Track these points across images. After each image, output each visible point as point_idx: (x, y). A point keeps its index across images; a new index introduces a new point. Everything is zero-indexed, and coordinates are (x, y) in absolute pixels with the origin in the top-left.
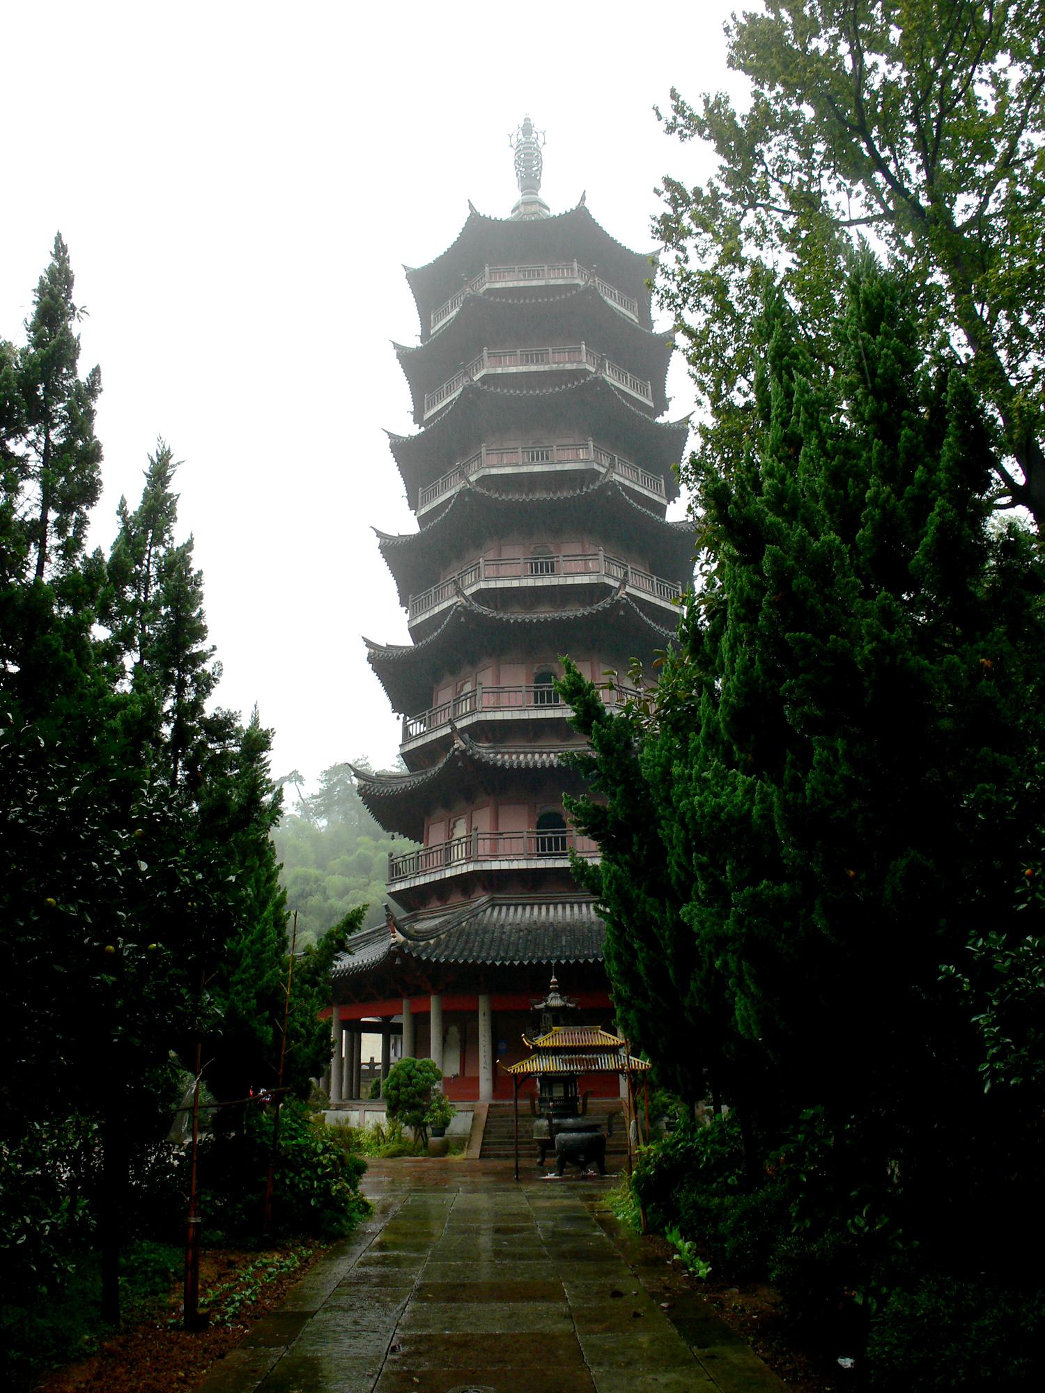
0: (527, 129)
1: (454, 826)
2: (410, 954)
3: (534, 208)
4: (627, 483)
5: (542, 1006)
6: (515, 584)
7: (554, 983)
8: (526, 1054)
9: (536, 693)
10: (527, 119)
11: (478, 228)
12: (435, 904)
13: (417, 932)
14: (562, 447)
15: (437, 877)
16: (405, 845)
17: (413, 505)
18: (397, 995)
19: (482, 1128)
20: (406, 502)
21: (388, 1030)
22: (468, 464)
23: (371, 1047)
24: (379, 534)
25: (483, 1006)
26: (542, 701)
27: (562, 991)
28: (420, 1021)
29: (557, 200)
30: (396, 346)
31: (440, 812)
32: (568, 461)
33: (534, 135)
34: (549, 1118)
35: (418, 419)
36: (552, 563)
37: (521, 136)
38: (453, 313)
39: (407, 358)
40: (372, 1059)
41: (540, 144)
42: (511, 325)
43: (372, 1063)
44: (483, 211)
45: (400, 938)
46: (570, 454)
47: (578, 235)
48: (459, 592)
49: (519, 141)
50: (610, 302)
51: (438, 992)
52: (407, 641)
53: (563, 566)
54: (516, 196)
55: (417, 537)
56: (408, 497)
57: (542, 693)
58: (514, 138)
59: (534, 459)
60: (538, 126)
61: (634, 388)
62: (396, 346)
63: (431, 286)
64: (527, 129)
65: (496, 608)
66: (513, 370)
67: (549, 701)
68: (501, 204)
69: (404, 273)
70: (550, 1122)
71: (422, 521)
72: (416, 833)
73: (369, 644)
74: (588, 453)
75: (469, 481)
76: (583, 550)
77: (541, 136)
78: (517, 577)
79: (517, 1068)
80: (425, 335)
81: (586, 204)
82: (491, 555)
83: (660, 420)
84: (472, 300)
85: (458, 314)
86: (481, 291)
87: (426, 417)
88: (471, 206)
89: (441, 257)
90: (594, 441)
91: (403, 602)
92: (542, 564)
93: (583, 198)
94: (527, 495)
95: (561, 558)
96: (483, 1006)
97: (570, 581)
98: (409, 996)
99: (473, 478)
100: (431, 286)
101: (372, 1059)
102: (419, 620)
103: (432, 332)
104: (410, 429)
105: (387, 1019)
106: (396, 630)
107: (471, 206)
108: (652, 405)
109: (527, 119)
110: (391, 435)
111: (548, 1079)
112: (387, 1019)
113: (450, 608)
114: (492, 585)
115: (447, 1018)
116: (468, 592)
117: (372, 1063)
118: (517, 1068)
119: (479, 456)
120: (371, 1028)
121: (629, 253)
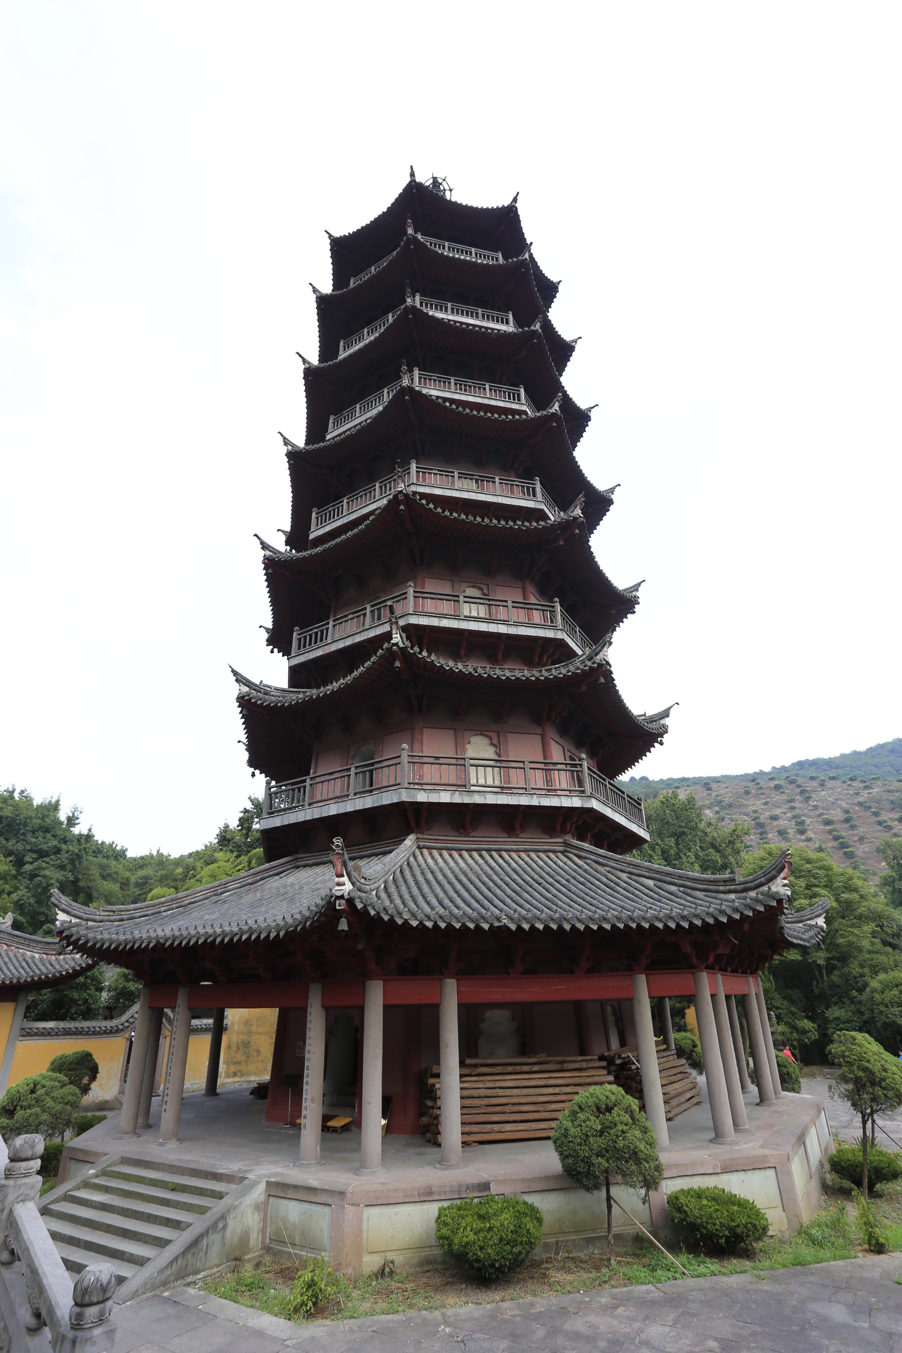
44: (337, 234)
69: (285, 450)
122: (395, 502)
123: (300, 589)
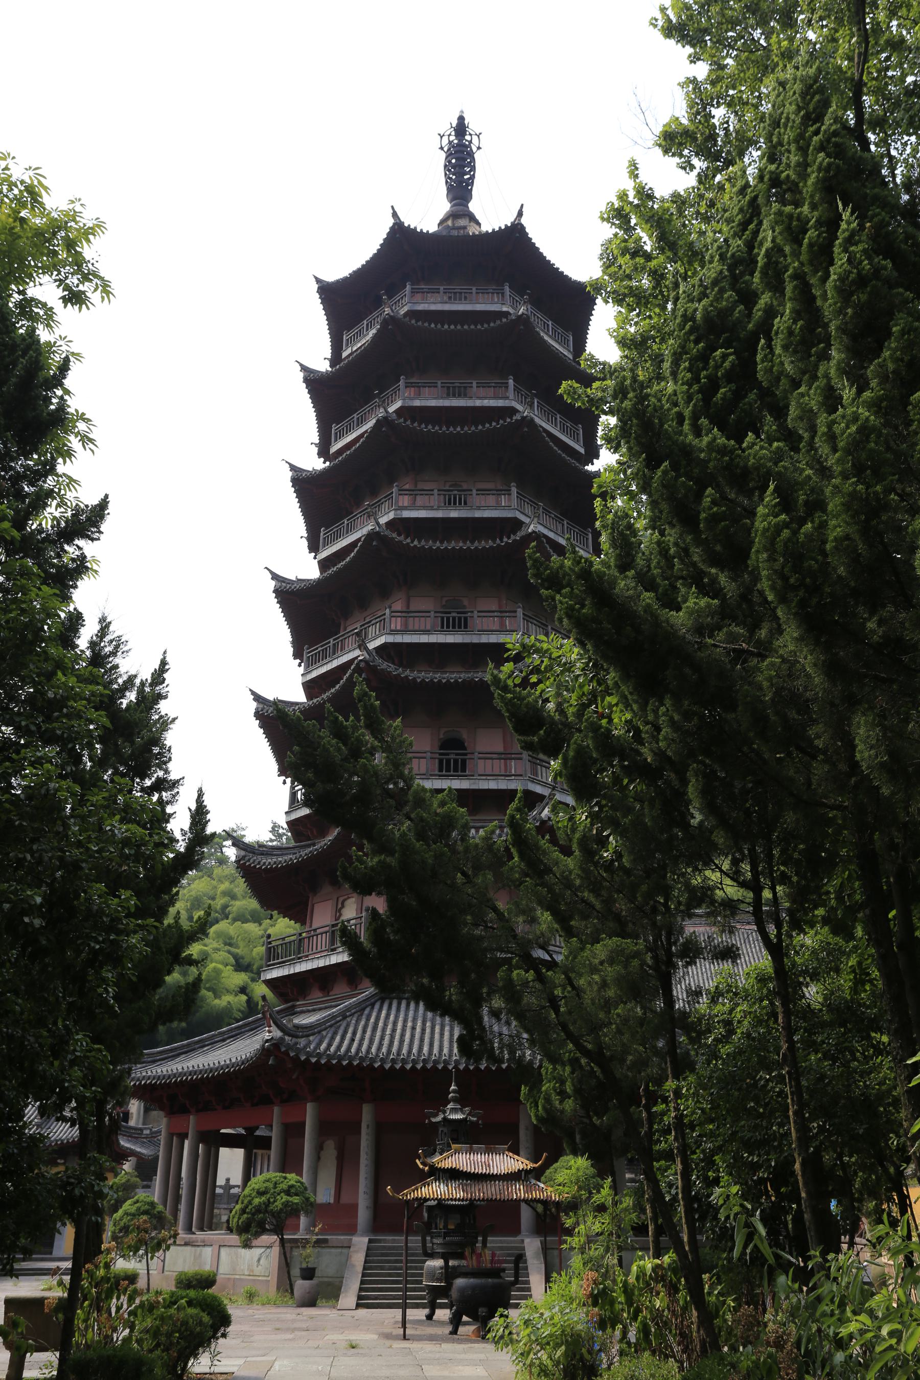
0: (461, 128)
1: (343, 906)
2: (286, 1053)
3: (462, 222)
4: (551, 535)
5: (440, 1118)
6: (424, 639)
7: (454, 1091)
8: (422, 1177)
9: (441, 762)
10: (461, 119)
11: (401, 237)
12: (316, 995)
13: (297, 1027)
14: (483, 492)
15: (321, 963)
16: (283, 927)
17: (314, 547)
18: (266, 1101)
19: (360, 1269)
20: (316, 450)
21: (252, 1145)
22: (378, 505)
23: (231, 1163)
24: (293, 468)
25: (367, 1114)
26: (448, 770)
27: (463, 1101)
28: (293, 1131)
29: (490, 213)
30: (304, 368)
31: (327, 889)
32: (488, 507)
33: (468, 138)
34: (445, 1257)
35: (323, 451)
36: (466, 619)
37: (452, 138)
38: (373, 332)
39: (316, 384)
40: (228, 1180)
41: (474, 149)
42: (434, 340)
43: (228, 1186)
44: (410, 221)
45: (278, 1034)
46: (491, 500)
47: (513, 254)
48: (362, 646)
49: (450, 142)
50: (546, 338)
51: (315, 1099)
52: (300, 697)
53: (477, 622)
54: (444, 206)
55: (318, 582)
56: (308, 539)
57: (448, 761)
58: (445, 141)
59: (451, 502)
60: (473, 125)
61: (563, 430)
62: (304, 368)
63: (344, 302)
64: (461, 128)
65: (401, 665)
66: (433, 403)
67: (456, 770)
68: (428, 213)
70: (446, 1262)
71: (324, 565)
72: (298, 911)
73: (257, 698)
74: (509, 500)
75: (378, 524)
76: (500, 606)
77: (475, 139)
78: (426, 632)
79: (411, 1194)
80: (335, 359)
81: (524, 221)
82: (398, 606)
83: (589, 468)
84: (390, 323)
85: (375, 336)
86: (402, 312)
87: (334, 449)
88: (395, 215)
89: (359, 269)
90: (524, 609)
91: (297, 654)
92: (454, 618)
93: (520, 214)
94: (442, 542)
95: (476, 614)
96: (367, 1114)
97: (484, 639)
98: (198, 1111)
99: (383, 520)
100: (344, 302)
101: (228, 1180)
102: (314, 674)
103: (344, 355)
104: (314, 463)
105: (250, 1130)
106: (288, 683)
107: (395, 215)
108: (582, 451)
109: (461, 119)
110: (293, 468)
111: (442, 1207)
112: (250, 1130)
113: (351, 662)
114: (399, 639)
115: (324, 1129)
116: (372, 646)
117: (228, 1186)
118: (411, 1194)
119: (389, 497)
120: (232, 1142)
121: (566, 279)
122: (385, 323)
123: (332, 395)
